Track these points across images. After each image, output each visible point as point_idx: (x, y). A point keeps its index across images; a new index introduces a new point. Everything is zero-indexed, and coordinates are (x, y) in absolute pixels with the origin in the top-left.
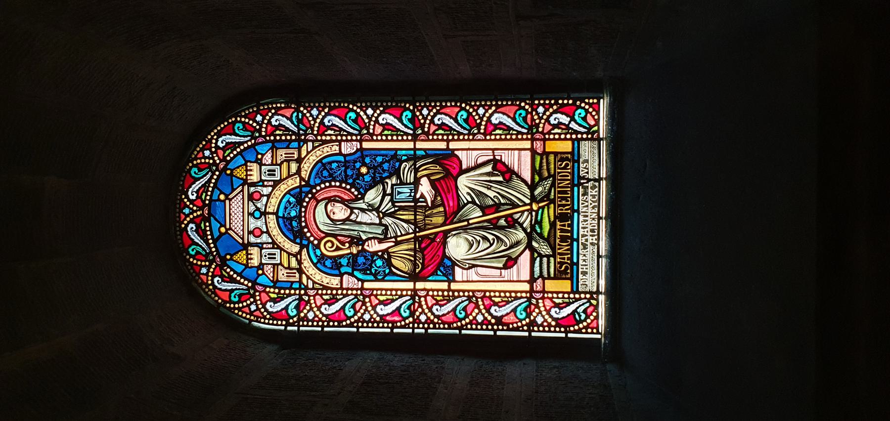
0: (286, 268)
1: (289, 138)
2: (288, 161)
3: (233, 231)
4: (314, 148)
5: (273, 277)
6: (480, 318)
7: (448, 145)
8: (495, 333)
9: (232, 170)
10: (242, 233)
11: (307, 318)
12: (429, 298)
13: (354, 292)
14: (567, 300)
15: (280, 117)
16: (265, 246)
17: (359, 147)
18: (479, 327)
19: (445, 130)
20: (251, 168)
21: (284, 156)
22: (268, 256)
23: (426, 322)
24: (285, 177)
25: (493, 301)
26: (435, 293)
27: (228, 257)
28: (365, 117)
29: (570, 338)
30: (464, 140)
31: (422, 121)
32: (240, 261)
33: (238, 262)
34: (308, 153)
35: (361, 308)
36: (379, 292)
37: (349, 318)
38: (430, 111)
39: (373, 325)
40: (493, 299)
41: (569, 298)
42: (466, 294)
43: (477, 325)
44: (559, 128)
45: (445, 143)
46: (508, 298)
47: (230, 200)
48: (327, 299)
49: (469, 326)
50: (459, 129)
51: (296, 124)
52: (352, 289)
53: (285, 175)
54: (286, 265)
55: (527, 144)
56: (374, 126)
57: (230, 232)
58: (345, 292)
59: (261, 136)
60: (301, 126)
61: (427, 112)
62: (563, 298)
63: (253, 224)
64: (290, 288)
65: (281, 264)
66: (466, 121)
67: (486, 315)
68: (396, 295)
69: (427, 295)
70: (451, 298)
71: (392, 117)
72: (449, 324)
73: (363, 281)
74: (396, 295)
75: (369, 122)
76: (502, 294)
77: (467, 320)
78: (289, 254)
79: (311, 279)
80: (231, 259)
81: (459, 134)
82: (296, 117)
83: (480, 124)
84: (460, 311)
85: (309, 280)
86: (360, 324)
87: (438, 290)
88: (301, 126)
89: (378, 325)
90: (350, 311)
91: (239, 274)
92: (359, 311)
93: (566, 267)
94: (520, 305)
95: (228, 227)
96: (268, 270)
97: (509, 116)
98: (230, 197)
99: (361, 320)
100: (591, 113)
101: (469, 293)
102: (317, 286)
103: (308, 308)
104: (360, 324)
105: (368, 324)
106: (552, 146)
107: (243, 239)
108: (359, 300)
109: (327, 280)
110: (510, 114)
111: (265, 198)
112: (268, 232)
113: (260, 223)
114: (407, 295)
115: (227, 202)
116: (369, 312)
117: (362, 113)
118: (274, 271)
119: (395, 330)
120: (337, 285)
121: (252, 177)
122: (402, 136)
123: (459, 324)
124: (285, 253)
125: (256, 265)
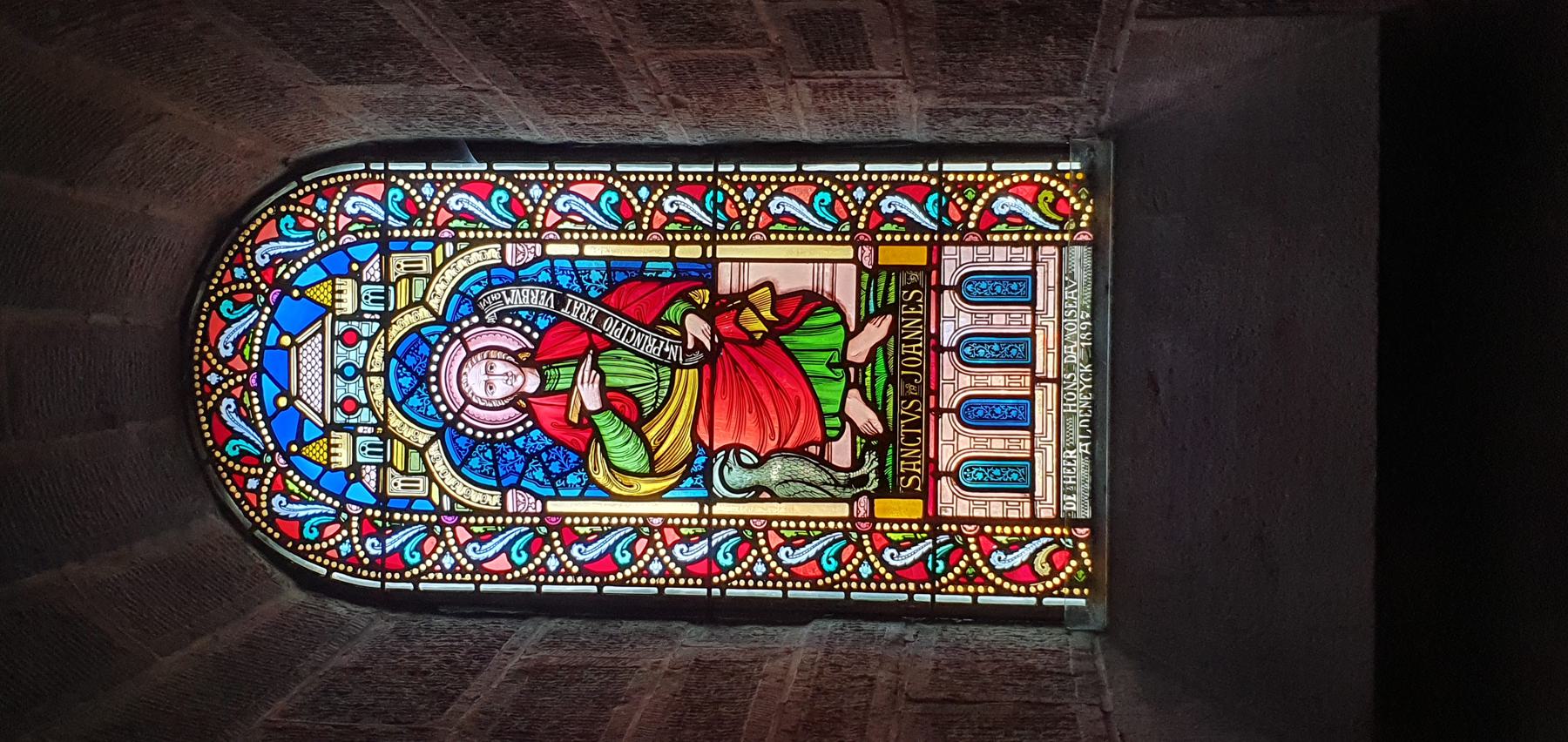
0: (402, 473)
1: (472, 235)
2: (409, 277)
3: (304, 402)
4: (456, 253)
5: (377, 486)
6: (760, 569)
7: (672, 251)
8: (477, 587)
9: (302, 289)
10: (320, 406)
11: (547, 568)
12: (460, 529)
13: (528, 520)
14: (492, 528)
15: (786, 199)
16: (360, 429)
17: (539, 254)
18: (449, 577)
19: (684, 224)
20: (342, 288)
21: (403, 266)
22: (368, 449)
23: (661, 575)
24: (403, 306)
25: (889, 539)
26: (887, 527)
27: (294, 448)
28: (634, 202)
29: (1048, 607)
30: (825, 242)
31: (744, 213)
32: (314, 458)
33: (310, 460)
34: (446, 260)
35: (644, 552)
36: (784, 524)
37: (622, 568)
38: (545, 190)
39: (878, 586)
40: (889, 535)
41: (494, 524)
42: (733, 522)
43: (756, 580)
44: (893, 223)
45: (699, 248)
46: (915, 533)
47: (299, 346)
48: (479, 533)
49: (1066, 591)
50: (601, 221)
51: (710, 209)
52: (523, 515)
53: (402, 303)
54: (401, 467)
55: (847, 251)
56: (545, 215)
57: (298, 403)
58: (509, 520)
59: (744, 229)
60: (720, 215)
61: (540, 192)
62: (590, 524)
63: (342, 389)
64: (409, 510)
65: (391, 464)
66: (1053, 206)
67: (459, 556)
68: (817, 528)
69: (769, 527)
70: (500, 529)
71: (906, 202)
72: (813, 580)
73: (544, 500)
74: (817, 528)
75: (643, 210)
76: (905, 526)
77: (634, 569)
78: (408, 446)
79: (449, 495)
80: (298, 453)
81: (816, 231)
82: (935, 202)
83: (642, 214)
84: (828, 558)
85: (445, 497)
86: (542, 578)
87: (788, 519)
88: (720, 215)
89: (888, 587)
90: (623, 555)
91: (315, 484)
92: (640, 557)
93: (916, 480)
94: (1039, 550)
95: (294, 393)
96: (370, 475)
97: (800, 201)
98: (299, 340)
99: (645, 572)
100: (841, 198)
101: (637, 518)
102: (459, 508)
103: (547, 548)
104: (542, 578)
105: (555, 578)
106: (889, 256)
107: (322, 415)
108: (640, 536)
109: (476, 497)
110: (801, 197)
111: (364, 344)
112: (369, 405)
113: (355, 389)
114: (628, 525)
115: (294, 349)
116: (661, 559)
117: (629, 195)
118: (378, 477)
119: (606, 589)
120: (497, 505)
121: (343, 305)
122: (806, 234)
123: (828, 580)
124: (400, 443)
125: (345, 465)
